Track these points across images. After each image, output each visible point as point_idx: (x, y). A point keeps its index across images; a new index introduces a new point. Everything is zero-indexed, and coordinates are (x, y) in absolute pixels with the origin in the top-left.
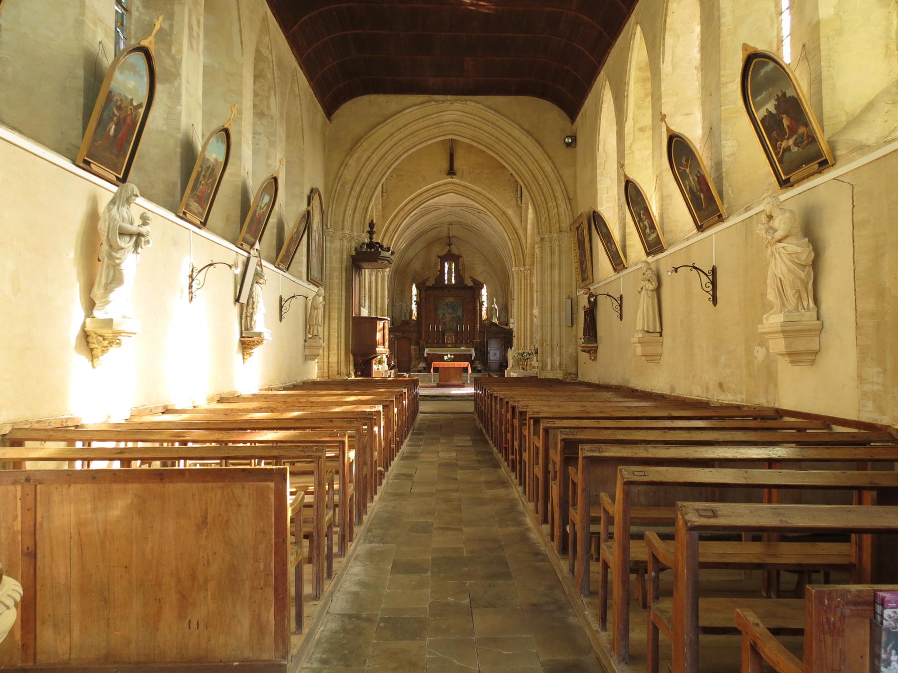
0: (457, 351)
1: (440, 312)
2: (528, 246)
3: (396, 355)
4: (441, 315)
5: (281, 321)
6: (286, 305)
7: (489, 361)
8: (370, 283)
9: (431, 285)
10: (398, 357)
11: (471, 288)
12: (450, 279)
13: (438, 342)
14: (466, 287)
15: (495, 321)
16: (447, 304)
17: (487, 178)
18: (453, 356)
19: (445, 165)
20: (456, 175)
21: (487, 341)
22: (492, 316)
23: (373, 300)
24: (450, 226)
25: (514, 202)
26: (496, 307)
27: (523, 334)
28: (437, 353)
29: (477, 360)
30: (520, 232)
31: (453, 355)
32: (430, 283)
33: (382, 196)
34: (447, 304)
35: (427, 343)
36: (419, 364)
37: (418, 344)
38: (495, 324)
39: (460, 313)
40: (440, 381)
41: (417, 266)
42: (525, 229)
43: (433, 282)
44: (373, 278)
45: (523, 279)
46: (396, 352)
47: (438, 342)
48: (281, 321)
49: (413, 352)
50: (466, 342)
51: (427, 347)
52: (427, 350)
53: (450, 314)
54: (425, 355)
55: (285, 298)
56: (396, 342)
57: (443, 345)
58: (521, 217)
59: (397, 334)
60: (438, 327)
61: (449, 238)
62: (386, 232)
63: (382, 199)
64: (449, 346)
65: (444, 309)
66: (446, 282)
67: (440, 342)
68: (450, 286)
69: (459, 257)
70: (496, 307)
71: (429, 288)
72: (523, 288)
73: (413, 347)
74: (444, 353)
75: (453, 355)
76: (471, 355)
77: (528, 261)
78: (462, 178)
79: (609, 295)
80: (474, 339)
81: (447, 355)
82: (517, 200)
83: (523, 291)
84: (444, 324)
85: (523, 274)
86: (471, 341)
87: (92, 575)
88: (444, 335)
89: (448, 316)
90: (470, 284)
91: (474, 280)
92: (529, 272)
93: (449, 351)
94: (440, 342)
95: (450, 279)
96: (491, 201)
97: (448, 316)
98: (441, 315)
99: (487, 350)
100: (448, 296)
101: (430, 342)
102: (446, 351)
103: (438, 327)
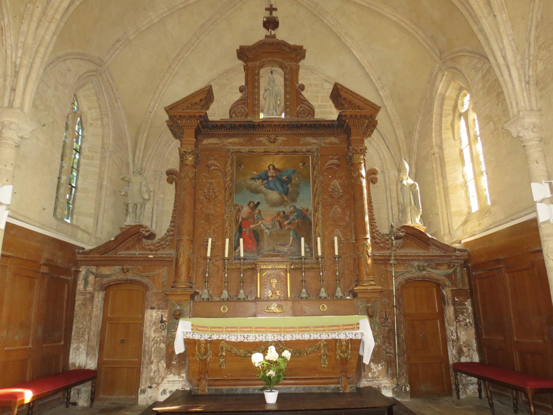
16: (264, 177)
28: (224, 336)
34: (264, 177)
50: (332, 295)
53: (274, 204)
56: (99, 297)
59: (105, 270)
64: (274, 307)
65: (256, 191)
74: (252, 338)
76: (356, 344)
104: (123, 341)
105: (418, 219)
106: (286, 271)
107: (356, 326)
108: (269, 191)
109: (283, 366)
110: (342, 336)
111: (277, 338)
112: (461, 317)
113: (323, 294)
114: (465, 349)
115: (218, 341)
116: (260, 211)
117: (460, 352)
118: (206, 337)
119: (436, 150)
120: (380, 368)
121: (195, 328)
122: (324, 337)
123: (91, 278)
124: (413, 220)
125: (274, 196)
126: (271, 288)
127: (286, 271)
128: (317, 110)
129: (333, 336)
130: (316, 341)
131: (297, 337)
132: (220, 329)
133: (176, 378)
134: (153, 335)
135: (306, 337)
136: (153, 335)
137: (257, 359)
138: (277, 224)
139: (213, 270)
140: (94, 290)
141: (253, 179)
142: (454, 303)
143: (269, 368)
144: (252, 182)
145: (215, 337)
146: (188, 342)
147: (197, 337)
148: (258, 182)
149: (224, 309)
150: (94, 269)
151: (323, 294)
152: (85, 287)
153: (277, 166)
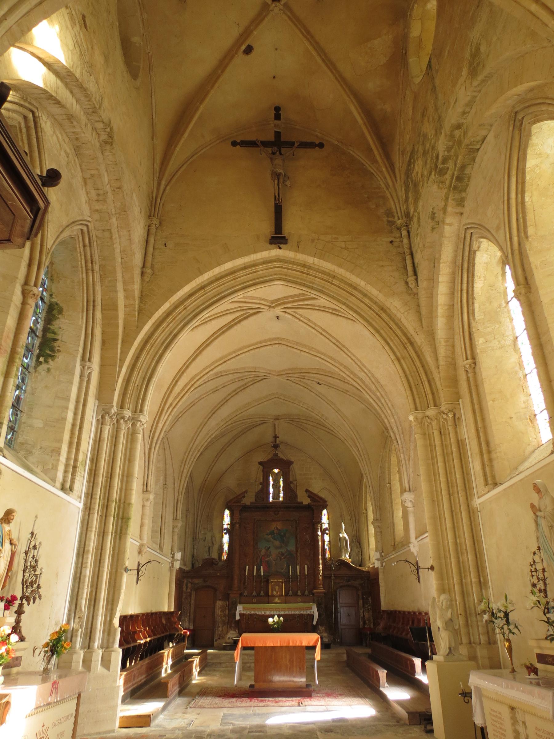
0: (290, 609)
1: (262, 546)
2: (442, 362)
3: (192, 617)
4: (263, 551)
5: (137, 583)
6: (143, 569)
7: (340, 627)
8: (98, 442)
9: (248, 503)
10: (194, 621)
11: (308, 508)
12: (276, 496)
13: (258, 595)
14: (300, 507)
15: (346, 557)
16: (272, 533)
17: (345, 248)
18: (281, 619)
19: (267, 228)
20: (286, 243)
21: (335, 592)
22: (341, 551)
23: (100, 480)
24: (277, 422)
25: (401, 287)
26: (347, 538)
27: (453, 561)
28: (256, 612)
29: (322, 625)
30: (420, 339)
31: (283, 616)
32: (249, 500)
33: (142, 274)
34: (272, 533)
35: (241, 595)
36: (227, 633)
37: (226, 597)
38: (344, 563)
39: (292, 547)
40: (256, 681)
41: (231, 482)
42: (431, 334)
43: (253, 500)
44: (107, 430)
45: (436, 433)
46: (192, 610)
47: (258, 595)
48: (137, 583)
49: (219, 612)
50: (303, 594)
51: (241, 603)
52: (240, 609)
53: (277, 548)
54: (238, 617)
55: (142, 563)
56: (193, 594)
57: (267, 598)
58: (419, 312)
59: (196, 581)
60: (259, 570)
61: (276, 447)
62: (145, 342)
63: (142, 281)
64: (277, 600)
65: (268, 541)
66: (271, 500)
67: (262, 593)
68: (276, 506)
69: (289, 463)
70: (347, 538)
71: (245, 508)
72: (439, 451)
73: (219, 604)
74: (268, 613)
75: (283, 616)
76: (312, 616)
77: (444, 394)
78: (298, 248)
79: (407, 561)
80: (315, 588)
81: (273, 616)
82: (407, 283)
83: (440, 459)
84: (268, 564)
85: (434, 423)
86: (311, 592)
87: (529, 445)
88: (267, 582)
89: (274, 552)
90: (306, 501)
91: (311, 495)
92: (451, 415)
93: (277, 609)
94: (262, 593)
95: (276, 496)
96: (355, 288)
97: (274, 552)
98: (263, 551)
99: (336, 608)
100: (274, 521)
101: (245, 594)
102: (271, 609)
103: (259, 570)
104: (204, 616)
105: (347, 556)
106: (282, 583)
107: (311, 608)
108: (275, 541)
109: (280, 623)
110: (305, 613)
111: (278, 613)
112: (366, 606)
113: (299, 593)
114: (367, 622)
115: (254, 614)
116: (270, 552)
117: (364, 623)
118: (249, 612)
119: (364, 511)
120: (323, 628)
121: (244, 608)
122: (298, 613)
123: (189, 585)
124: (345, 556)
125: (277, 543)
126: (275, 590)
127: (282, 583)
128: (299, 497)
129: (301, 612)
130: (294, 615)
131: (286, 613)
132: (254, 609)
133: (234, 632)
134: (220, 613)
135: (290, 613)
136: (220, 613)
137: (270, 620)
138: (279, 558)
139: (39, 323)
140: (191, 591)
141: (267, 534)
142: (363, 599)
143: (275, 624)
144: (266, 536)
145: (252, 612)
146: (241, 615)
147: (245, 612)
148: (270, 536)
149: (254, 600)
150: (190, 580)
151: (299, 593)
152: (186, 590)
153: (279, 528)
